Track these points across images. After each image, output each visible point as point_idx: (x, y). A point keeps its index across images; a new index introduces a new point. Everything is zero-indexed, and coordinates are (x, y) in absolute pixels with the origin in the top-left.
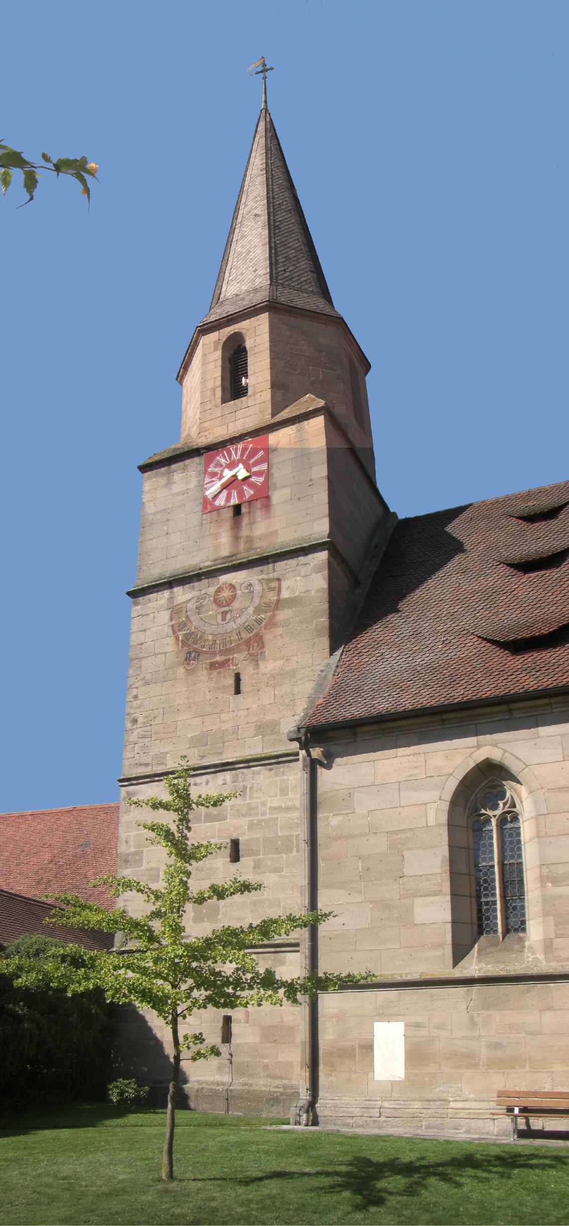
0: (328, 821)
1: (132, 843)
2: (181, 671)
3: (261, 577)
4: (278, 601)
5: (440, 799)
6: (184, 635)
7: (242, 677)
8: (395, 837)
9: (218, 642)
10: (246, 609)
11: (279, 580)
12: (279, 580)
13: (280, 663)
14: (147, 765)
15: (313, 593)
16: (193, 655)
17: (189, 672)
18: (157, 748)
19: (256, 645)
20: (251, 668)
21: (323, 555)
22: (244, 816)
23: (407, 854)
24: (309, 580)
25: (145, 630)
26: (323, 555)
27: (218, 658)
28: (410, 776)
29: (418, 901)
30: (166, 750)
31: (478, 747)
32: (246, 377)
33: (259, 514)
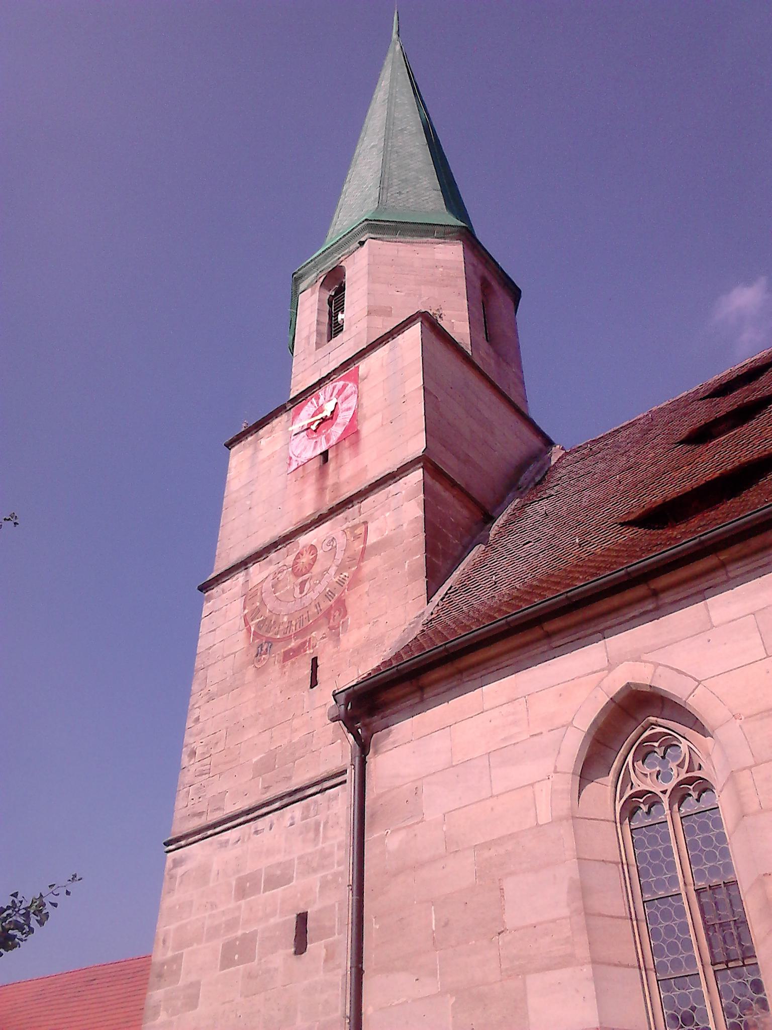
0: (384, 843)
1: (170, 943)
2: (251, 670)
3: (344, 527)
4: (364, 549)
5: (555, 772)
6: (258, 624)
7: (319, 662)
8: (486, 854)
9: (294, 623)
10: (327, 570)
12: (365, 523)
13: (366, 629)
14: (200, 814)
15: (405, 526)
16: (264, 649)
17: (260, 671)
18: (217, 786)
19: (337, 614)
20: (331, 646)
22: (315, 871)
23: (509, 885)
24: (401, 512)
25: (214, 630)
26: (417, 475)
27: (293, 644)
28: (505, 739)
29: (535, 982)
30: (225, 788)
31: (611, 667)
32: (343, 312)
33: (346, 454)
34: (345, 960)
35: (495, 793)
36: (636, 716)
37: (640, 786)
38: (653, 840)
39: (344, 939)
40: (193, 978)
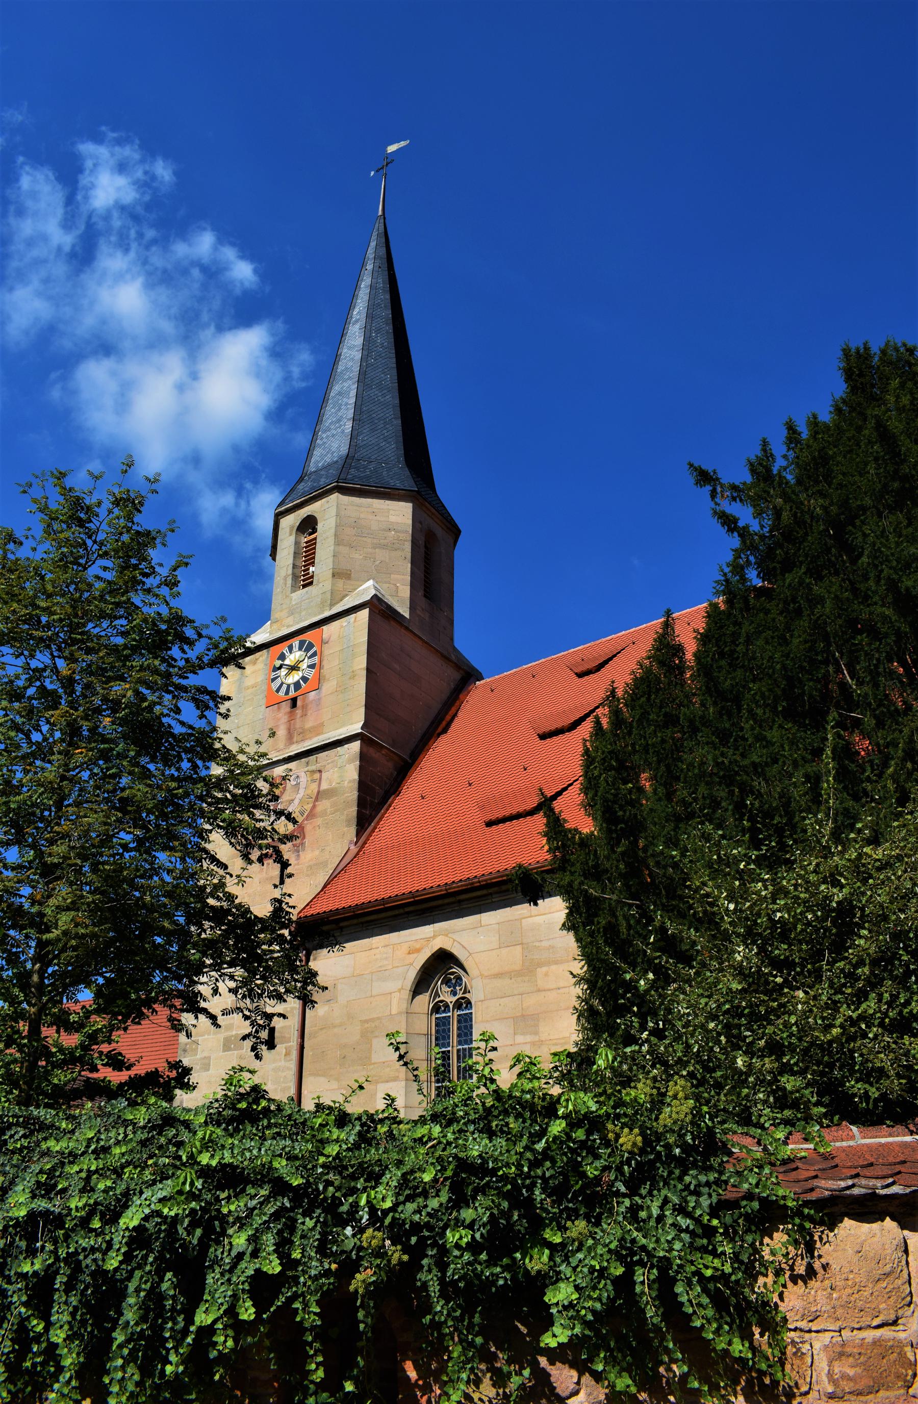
11: (320, 771)
12: (320, 771)
13: (317, 853)
21: (356, 746)
34: (295, 1054)
35: (374, 993)
36: (441, 966)
37: (442, 998)
38: (444, 1024)
39: (294, 1043)
40: (206, 1054)
